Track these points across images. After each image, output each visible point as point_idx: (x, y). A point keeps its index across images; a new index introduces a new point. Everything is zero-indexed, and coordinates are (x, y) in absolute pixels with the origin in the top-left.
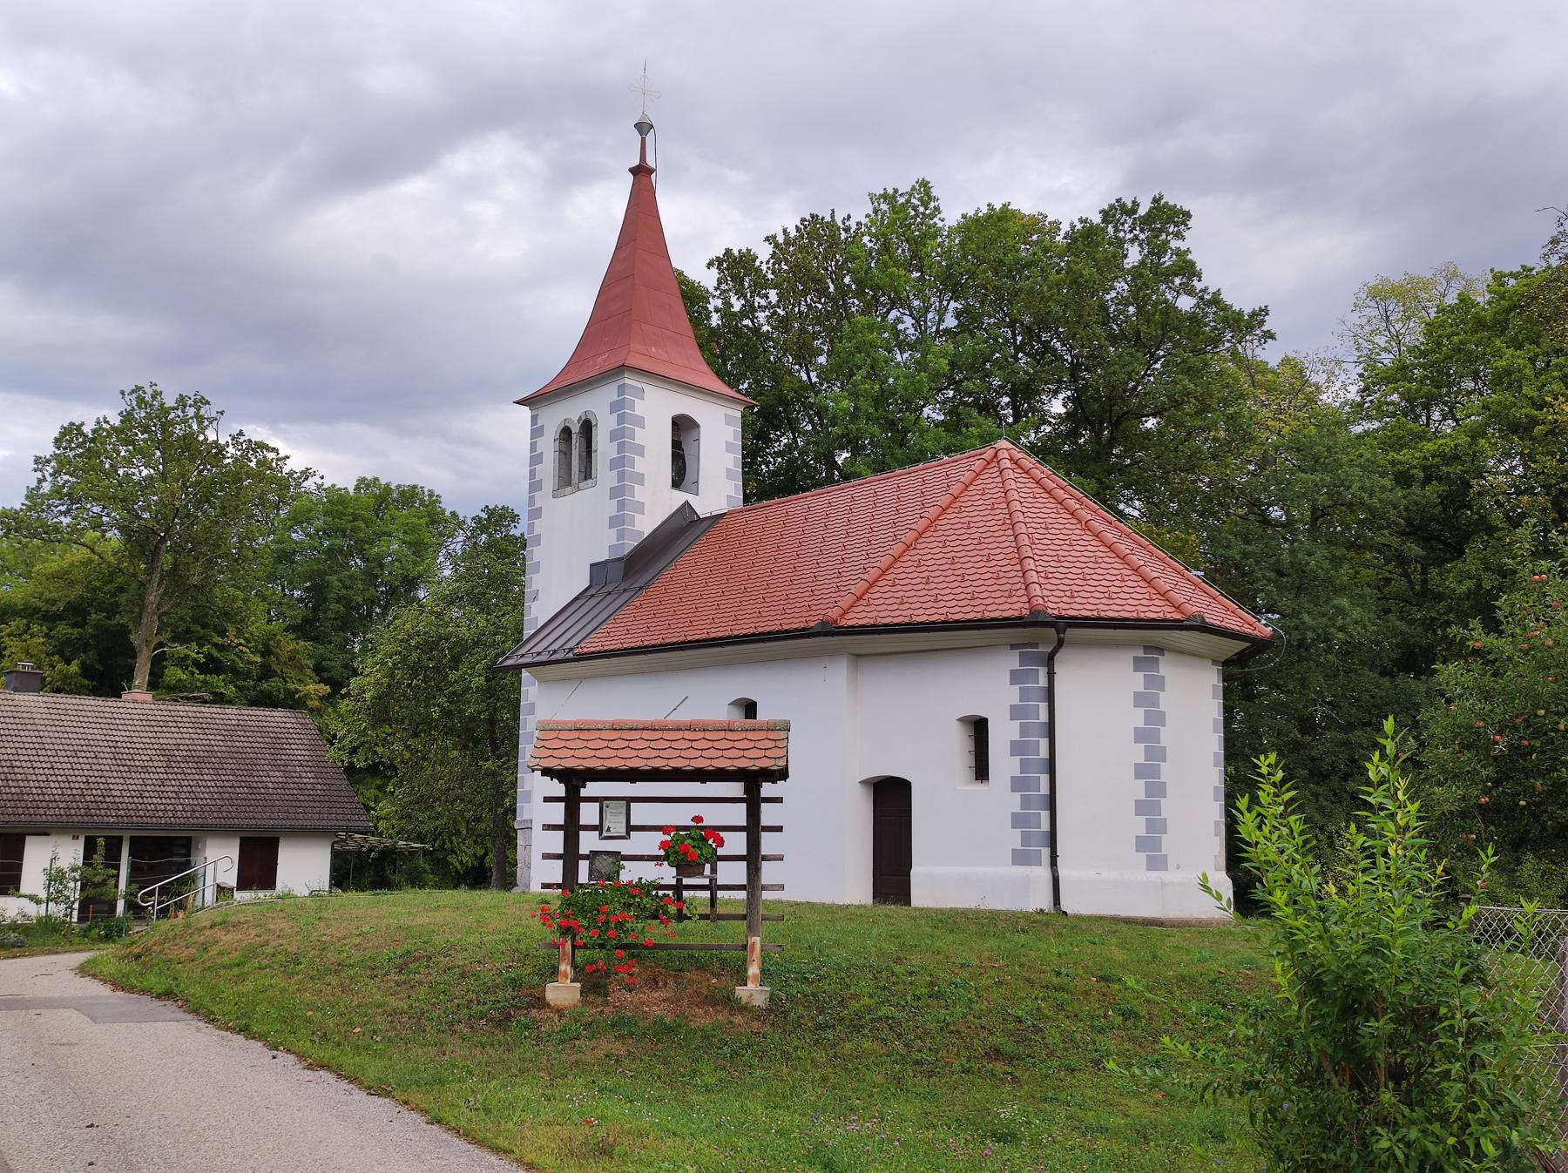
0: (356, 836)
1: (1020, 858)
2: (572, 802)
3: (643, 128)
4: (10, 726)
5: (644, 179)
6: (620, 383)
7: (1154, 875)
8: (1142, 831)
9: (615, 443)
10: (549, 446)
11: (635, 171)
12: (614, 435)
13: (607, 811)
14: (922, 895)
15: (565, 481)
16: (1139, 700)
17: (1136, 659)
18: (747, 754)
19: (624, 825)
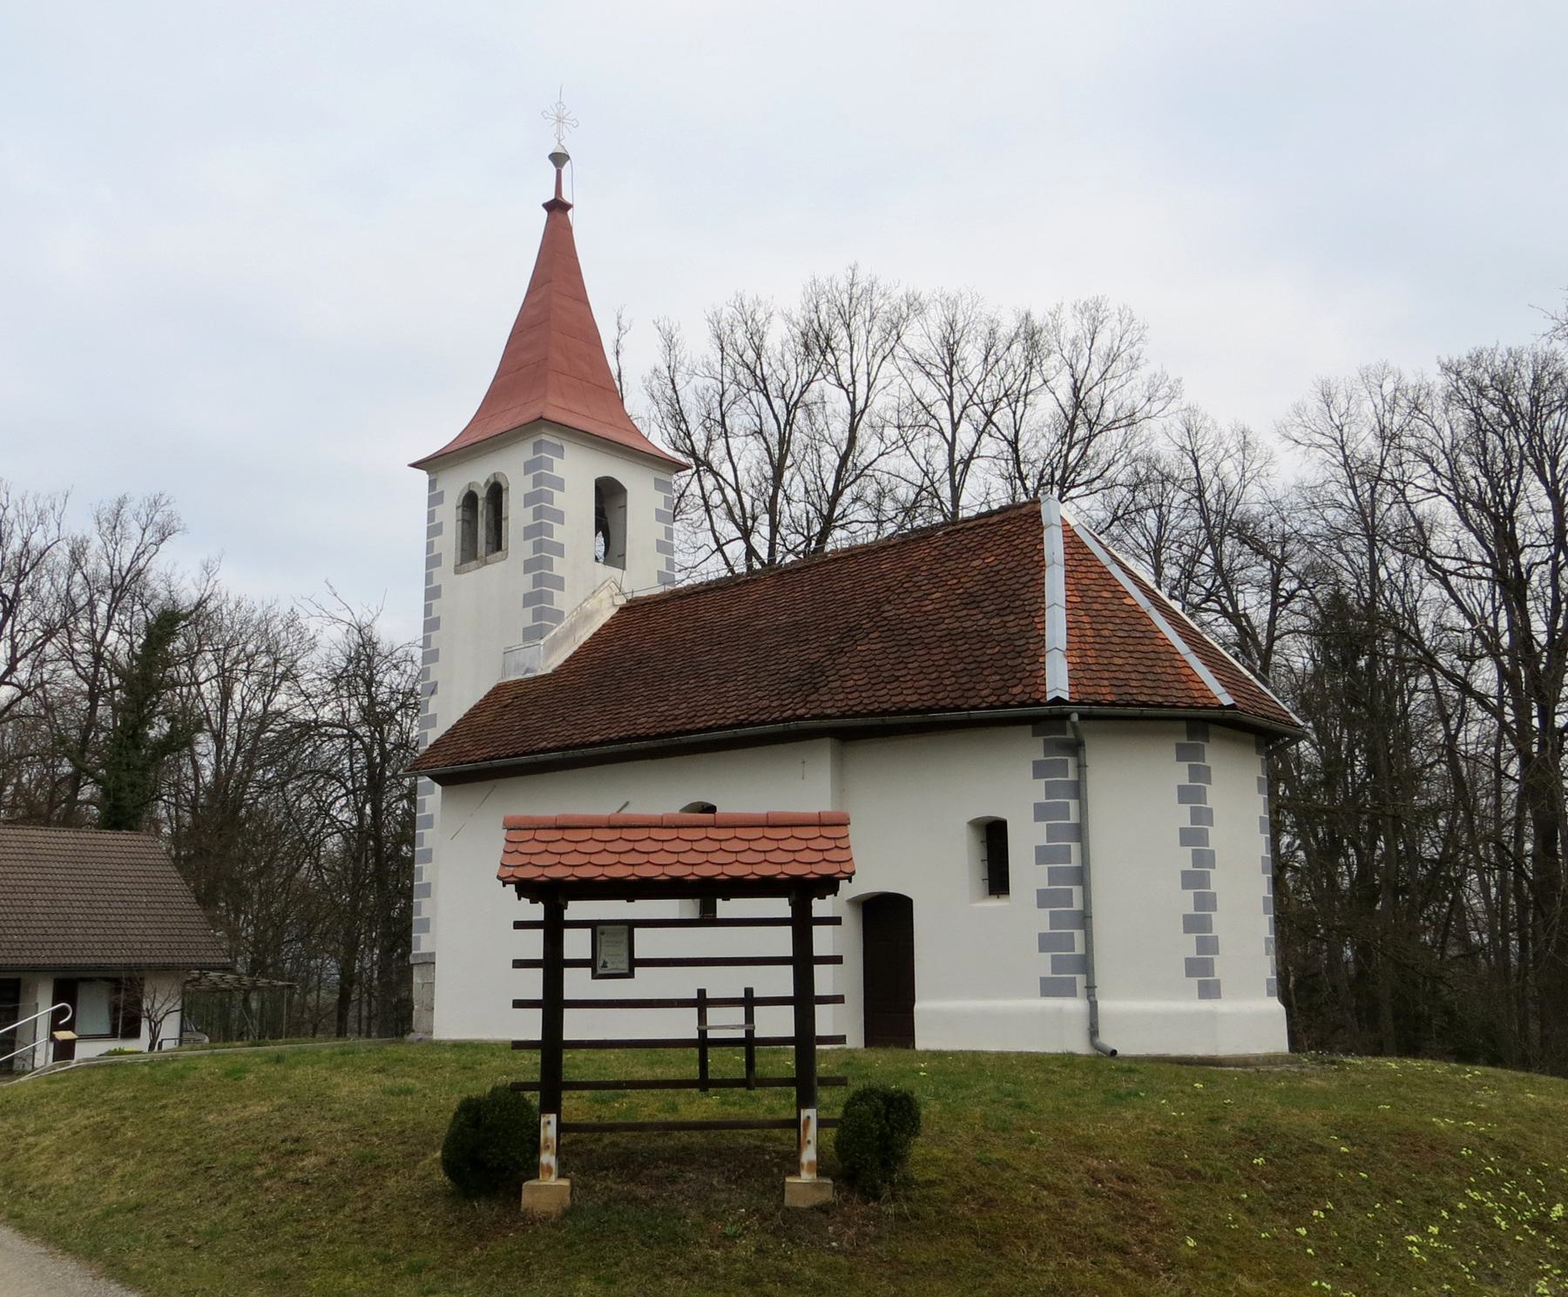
0: (211, 974)
1: (1050, 988)
2: (554, 928)
3: (559, 159)
4: (56, 871)
5: (559, 216)
6: (537, 439)
7: (1207, 1005)
8: (1192, 953)
9: (531, 509)
10: (450, 514)
11: (547, 206)
12: (529, 500)
13: (602, 939)
14: (925, 1039)
15: (469, 553)
16: (1186, 795)
17: (1180, 747)
18: (565, 860)
19: (627, 961)
